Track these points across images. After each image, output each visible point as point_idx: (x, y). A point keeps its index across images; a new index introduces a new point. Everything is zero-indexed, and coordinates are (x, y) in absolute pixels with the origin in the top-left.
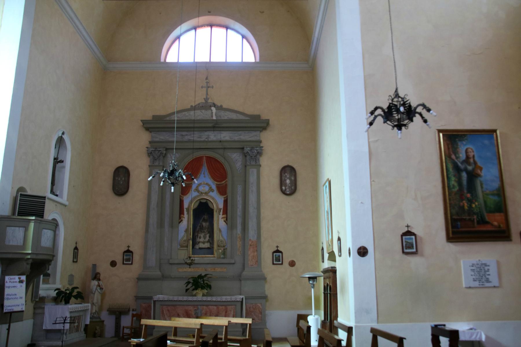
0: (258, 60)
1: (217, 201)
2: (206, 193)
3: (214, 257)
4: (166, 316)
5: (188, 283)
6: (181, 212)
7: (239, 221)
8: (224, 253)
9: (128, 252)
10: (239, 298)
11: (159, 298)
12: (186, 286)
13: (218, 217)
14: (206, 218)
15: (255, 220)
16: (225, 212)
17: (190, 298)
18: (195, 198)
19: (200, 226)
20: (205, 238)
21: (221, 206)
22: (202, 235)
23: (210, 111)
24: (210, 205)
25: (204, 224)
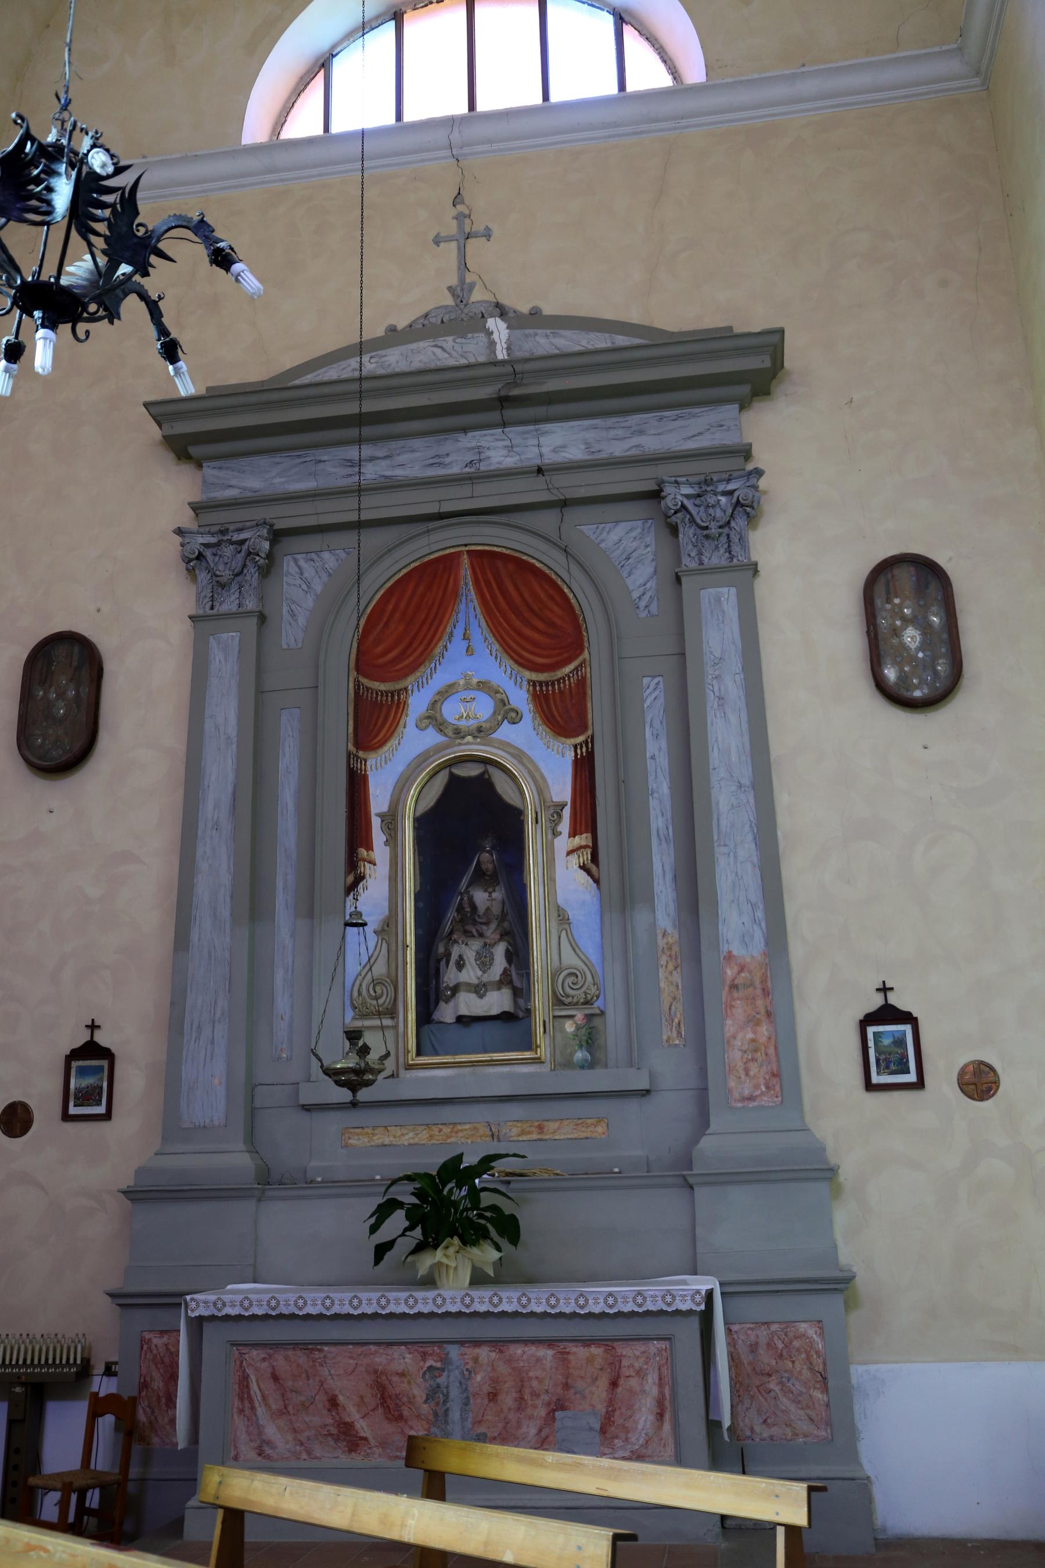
0: (695, 72)
1: (540, 767)
2: (480, 732)
3: (538, 1061)
4: (260, 1411)
5: (384, 1211)
6: (357, 835)
7: (662, 862)
8: (590, 1039)
9: (92, 1053)
10: (691, 1288)
11: (246, 1300)
12: (374, 1229)
13: (549, 851)
14: (488, 867)
15: (747, 849)
16: (585, 814)
17: (398, 1301)
18: (423, 758)
19: (460, 909)
20: (484, 962)
21: (562, 789)
22: (469, 951)
23: (482, 337)
24: (502, 786)
25: (480, 897)
